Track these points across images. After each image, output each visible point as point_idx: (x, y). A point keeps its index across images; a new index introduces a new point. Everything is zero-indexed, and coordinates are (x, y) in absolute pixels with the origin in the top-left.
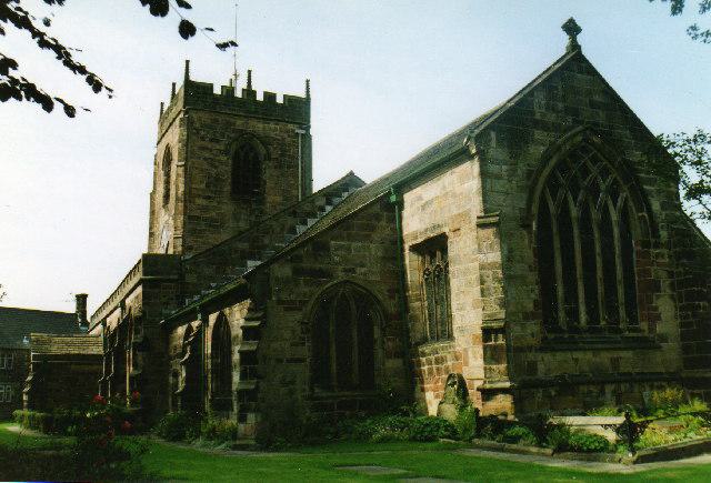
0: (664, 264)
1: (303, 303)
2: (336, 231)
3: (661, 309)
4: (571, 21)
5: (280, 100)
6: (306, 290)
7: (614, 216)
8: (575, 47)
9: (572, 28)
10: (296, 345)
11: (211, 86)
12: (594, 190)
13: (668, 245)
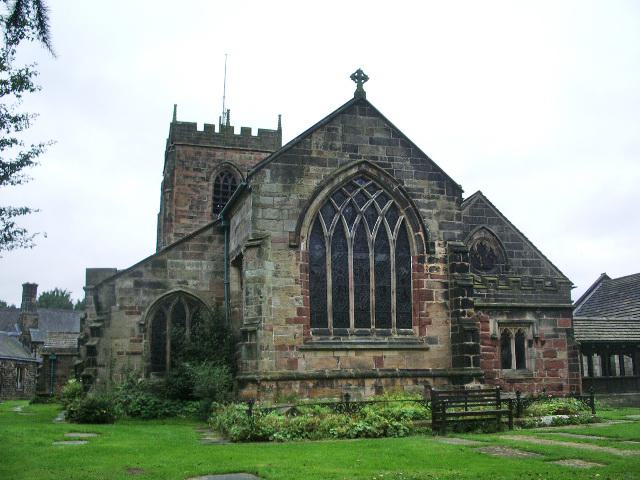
0: (438, 277)
1: (142, 309)
2: (173, 252)
3: (432, 315)
4: (359, 72)
5: (255, 133)
6: (145, 298)
7: (392, 237)
8: (360, 95)
9: (359, 77)
10: (135, 341)
11: (194, 125)
12: (372, 215)
13: (444, 261)
